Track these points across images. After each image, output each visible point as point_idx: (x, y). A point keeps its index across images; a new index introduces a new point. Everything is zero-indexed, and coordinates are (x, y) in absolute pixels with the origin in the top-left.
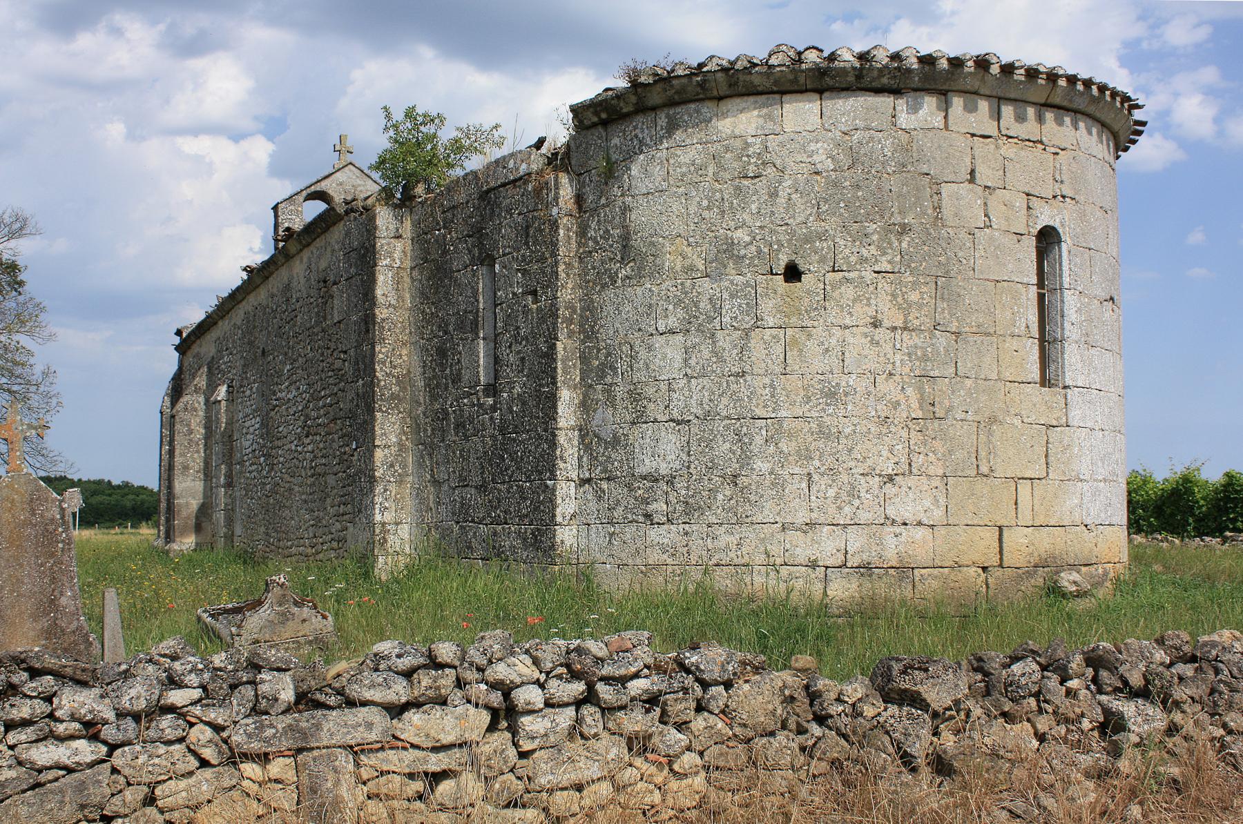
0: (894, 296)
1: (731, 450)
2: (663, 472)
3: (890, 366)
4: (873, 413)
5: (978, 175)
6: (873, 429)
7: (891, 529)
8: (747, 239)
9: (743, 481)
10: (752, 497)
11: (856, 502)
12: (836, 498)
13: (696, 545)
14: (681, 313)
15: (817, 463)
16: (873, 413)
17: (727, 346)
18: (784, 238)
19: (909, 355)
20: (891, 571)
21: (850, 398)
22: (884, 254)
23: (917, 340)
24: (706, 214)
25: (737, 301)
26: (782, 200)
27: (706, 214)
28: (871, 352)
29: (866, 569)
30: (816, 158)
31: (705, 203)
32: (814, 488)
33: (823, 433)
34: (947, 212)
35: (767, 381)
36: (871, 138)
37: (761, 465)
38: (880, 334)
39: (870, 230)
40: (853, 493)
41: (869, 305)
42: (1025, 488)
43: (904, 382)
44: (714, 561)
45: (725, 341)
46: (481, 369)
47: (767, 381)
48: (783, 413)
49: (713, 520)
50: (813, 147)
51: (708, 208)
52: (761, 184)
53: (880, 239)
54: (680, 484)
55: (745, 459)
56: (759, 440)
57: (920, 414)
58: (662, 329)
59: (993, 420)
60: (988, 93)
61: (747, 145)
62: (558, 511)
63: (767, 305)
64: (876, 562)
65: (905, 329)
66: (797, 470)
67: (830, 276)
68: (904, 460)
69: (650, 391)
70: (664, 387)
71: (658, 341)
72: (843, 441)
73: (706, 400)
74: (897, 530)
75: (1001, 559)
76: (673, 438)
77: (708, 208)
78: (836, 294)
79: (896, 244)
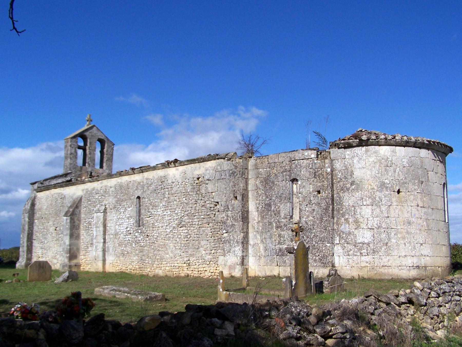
1: (385, 236)
2: (366, 242)
7: (422, 257)
8: (388, 182)
9: (389, 244)
13: (376, 260)
14: (370, 200)
15: (406, 240)
17: (384, 209)
24: (377, 175)
25: (386, 198)
26: (397, 173)
27: (377, 175)
28: (417, 212)
29: (418, 267)
30: (404, 163)
31: (377, 172)
33: (408, 233)
34: (430, 178)
35: (394, 219)
37: (393, 241)
40: (414, 248)
44: (382, 265)
45: (384, 208)
46: (58, 182)
47: (394, 219)
48: (399, 227)
49: (381, 254)
50: (403, 160)
51: (378, 173)
52: (392, 168)
53: (418, 185)
54: (371, 245)
55: (389, 239)
56: (393, 234)
57: (426, 228)
58: (365, 204)
61: (388, 158)
63: (394, 200)
64: (420, 265)
65: (423, 207)
66: (402, 242)
68: (424, 240)
69: (361, 220)
70: (366, 219)
71: (364, 207)
73: (378, 223)
76: (369, 233)
77: (378, 173)
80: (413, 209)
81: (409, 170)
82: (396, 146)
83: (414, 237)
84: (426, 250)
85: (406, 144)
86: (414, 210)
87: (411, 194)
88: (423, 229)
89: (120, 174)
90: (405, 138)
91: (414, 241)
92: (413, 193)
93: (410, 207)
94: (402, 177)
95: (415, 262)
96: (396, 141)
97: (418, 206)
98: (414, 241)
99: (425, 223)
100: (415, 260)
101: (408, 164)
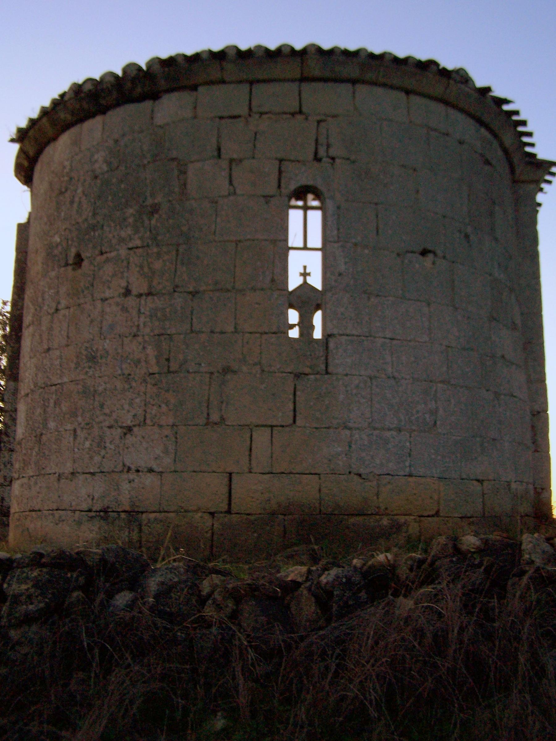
0: (141, 267)
3: (135, 329)
4: (120, 372)
5: (223, 150)
6: (118, 387)
7: (125, 476)
10: (47, 453)
11: (103, 452)
12: (90, 449)
15: (80, 419)
16: (120, 372)
23: (158, 302)
38: (131, 301)
40: (101, 443)
41: (122, 278)
42: (261, 438)
43: (145, 341)
48: (66, 380)
52: (68, 194)
57: (155, 369)
59: (227, 370)
65: (149, 294)
67: (99, 259)
68: (140, 412)
72: (97, 398)
74: (131, 476)
75: (230, 504)
79: (147, 222)
82: (82, 120)
83: (102, 406)
87: (108, 260)
91: (101, 418)
92: (113, 254)
93: (99, 304)
95: (96, 496)
98: (101, 418)
99: (150, 350)
100: (98, 487)
101: (109, 164)
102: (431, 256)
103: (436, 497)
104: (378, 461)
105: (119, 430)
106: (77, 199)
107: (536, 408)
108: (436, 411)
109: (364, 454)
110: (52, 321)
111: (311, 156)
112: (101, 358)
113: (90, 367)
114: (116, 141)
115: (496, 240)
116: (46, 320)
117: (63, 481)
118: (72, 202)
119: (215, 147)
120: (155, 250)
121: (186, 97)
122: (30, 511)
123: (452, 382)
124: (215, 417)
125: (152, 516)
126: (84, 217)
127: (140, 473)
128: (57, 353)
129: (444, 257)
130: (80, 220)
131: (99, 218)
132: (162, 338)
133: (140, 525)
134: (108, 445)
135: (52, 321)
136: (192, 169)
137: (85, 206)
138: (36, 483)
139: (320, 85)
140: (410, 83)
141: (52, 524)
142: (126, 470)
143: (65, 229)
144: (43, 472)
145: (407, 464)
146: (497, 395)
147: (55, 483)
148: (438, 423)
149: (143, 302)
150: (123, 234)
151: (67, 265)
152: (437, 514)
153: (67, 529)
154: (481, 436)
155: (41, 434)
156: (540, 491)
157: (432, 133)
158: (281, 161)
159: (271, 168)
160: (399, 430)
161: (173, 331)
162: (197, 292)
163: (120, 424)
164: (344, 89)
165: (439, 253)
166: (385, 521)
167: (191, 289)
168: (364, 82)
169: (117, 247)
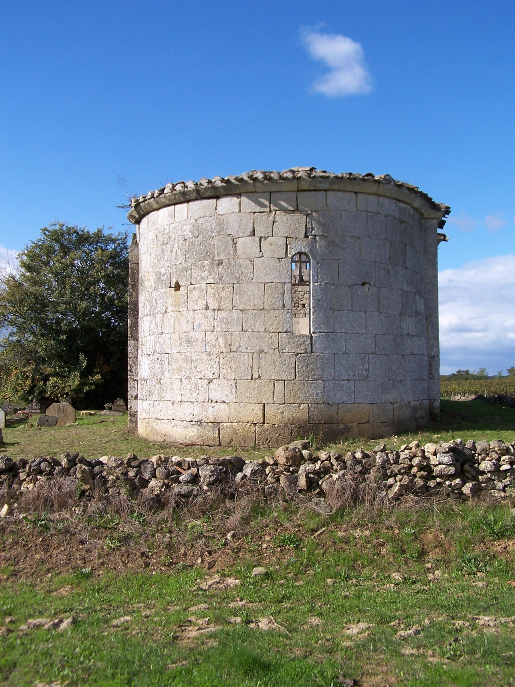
3: (212, 328)
7: (210, 404)
10: (165, 389)
12: (190, 389)
18: (174, 271)
19: (221, 322)
20: (210, 424)
21: (196, 343)
22: (211, 275)
28: (204, 321)
32: (183, 385)
36: (207, 221)
38: (209, 313)
39: (205, 264)
40: (196, 387)
41: (204, 299)
43: (218, 335)
46: (147, 367)
48: (174, 351)
50: (185, 227)
52: (169, 246)
53: (210, 268)
60: (261, 191)
62: (129, 393)
64: (204, 419)
65: (218, 310)
66: (177, 377)
74: (213, 404)
75: (264, 420)
78: (192, 295)
79: (216, 269)
80: (196, 316)
81: (192, 244)
83: (196, 367)
84: (221, 391)
85: (185, 198)
86: (198, 316)
88: (215, 351)
89: (309, 278)
90: (179, 188)
91: (196, 374)
92: (198, 286)
93: (191, 312)
94: (181, 259)
96: (165, 197)
97: (207, 308)
98: (196, 374)
99: (220, 340)
101: (192, 233)
102: (367, 285)
103: (367, 413)
104: (338, 397)
105: (206, 381)
106: (175, 250)
107: (433, 354)
108: (369, 369)
109: (330, 393)
110: (163, 317)
111: (303, 235)
112: (194, 342)
113: (188, 346)
114: (196, 220)
115: (406, 268)
116: (159, 317)
117: (175, 405)
118: (172, 251)
119: (252, 230)
120: (222, 286)
121: (235, 200)
122: (156, 419)
123: (378, 353)
124: (256, 376)
125: (225, 424)
126: (180, 262)
127: (218, 403)
128: (168, 336)
129: (375, 285)
130: (177, 263)
131: (189, 264)
132: (227, 333)
133: (219, 429)
134: (200, 388)
135: (163, 317)
136: (240, 241)
137: (180, 256)
138: (158, 405)
139: (309, 193)
140: (358, 189)
141: (170, 427)
142: (210, 401)
143: (168, 266)
144: (163, 399)
145: (353, 397)
146: (403, 356)
147: (171, 406)
148: (369, 375)
149: (216, 314)
150: (203, 275)
151: (170, 287)
152: (368, 422)
153: (179, 430)
154: (393, 380)
155: (161, 379)
156: (433, 401)
157: (369, 214)
158: (287, 238)
159: (282, 242)
160: (349, 380)
161: (233, 330)
162: (245, 310)
163: (206, 377)
164: (321, 195)
165: (372, 284)
166: (341, 426)
167: (241, 308)
168: (330, 190)
169: (200, 282)
